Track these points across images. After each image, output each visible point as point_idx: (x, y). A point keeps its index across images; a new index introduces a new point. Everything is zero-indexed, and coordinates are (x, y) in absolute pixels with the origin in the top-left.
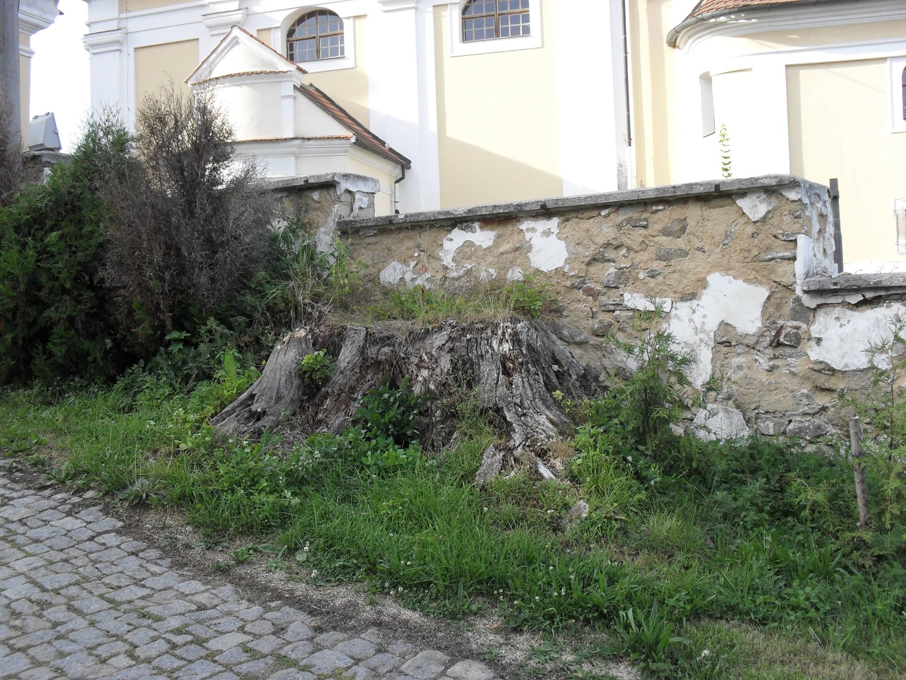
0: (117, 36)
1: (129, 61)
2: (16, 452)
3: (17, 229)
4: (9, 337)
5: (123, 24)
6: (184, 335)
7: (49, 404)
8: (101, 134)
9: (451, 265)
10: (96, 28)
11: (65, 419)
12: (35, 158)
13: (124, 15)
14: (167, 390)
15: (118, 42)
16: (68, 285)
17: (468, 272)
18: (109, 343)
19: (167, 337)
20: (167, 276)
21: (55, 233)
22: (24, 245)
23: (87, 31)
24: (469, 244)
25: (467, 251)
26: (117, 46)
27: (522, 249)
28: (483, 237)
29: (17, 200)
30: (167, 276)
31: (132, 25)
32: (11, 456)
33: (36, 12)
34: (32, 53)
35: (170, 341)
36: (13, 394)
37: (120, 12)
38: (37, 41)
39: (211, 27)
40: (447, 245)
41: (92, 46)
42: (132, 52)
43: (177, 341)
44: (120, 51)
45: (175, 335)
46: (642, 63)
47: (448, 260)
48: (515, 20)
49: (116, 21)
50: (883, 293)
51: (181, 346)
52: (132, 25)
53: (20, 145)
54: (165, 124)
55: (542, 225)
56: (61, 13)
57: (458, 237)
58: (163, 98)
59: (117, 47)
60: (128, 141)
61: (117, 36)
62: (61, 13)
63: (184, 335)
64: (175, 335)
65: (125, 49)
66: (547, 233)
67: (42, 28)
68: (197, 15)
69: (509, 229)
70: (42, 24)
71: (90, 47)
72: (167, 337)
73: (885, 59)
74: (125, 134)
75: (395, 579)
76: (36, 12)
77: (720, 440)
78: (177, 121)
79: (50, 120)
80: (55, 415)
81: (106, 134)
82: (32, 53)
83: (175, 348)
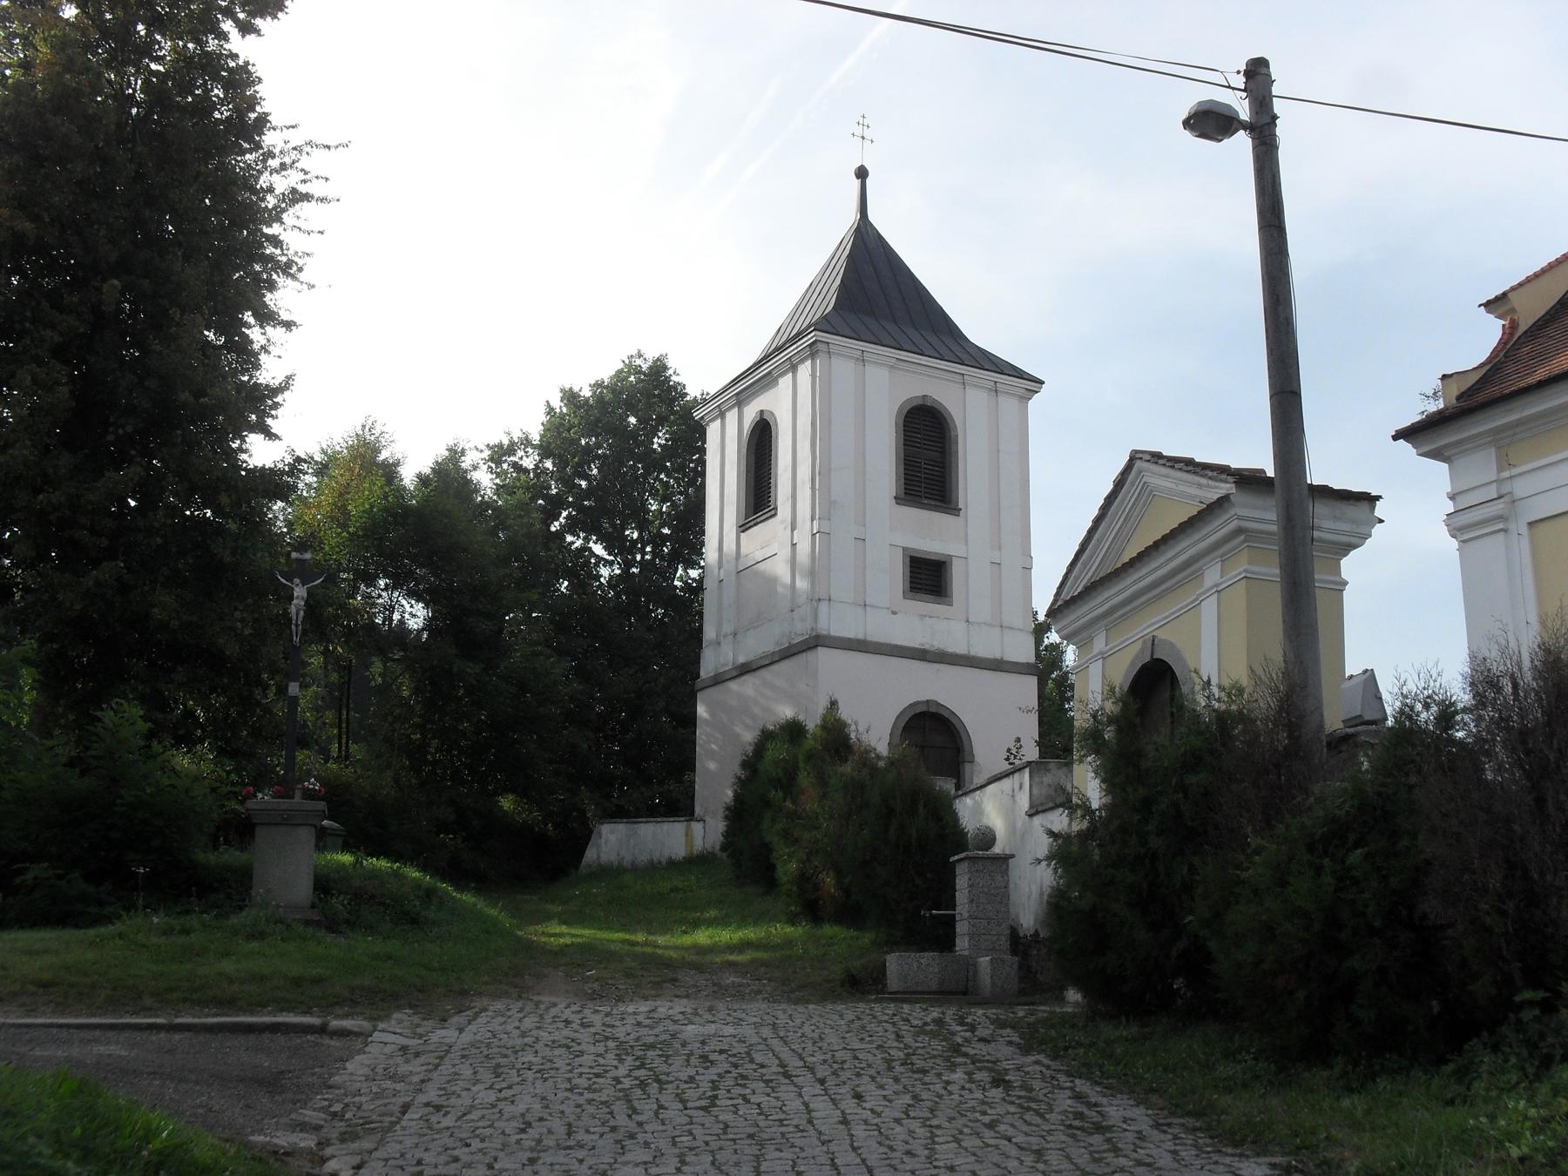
2: (1298, 1148)
3: (1311, 848)
4: (1301, 995)
5: (1506, 488)
6: (1541, 994)
7: (1351, 1090)
8: (1419, 707)
10: (1465, 501)
11: (1368, 1112)
12: (1346, 738)
13: (1506, 474)
14: (1514, 1078)
15: (1500, 518)
16: (1377, 924)
18: (1436, 1006)
19: (1517, 999)
20: (1510, 906)
21: (1359, 851)
22: (1319, 870)
23: (1450, 507)
26: (1499, 523)
29: (1309, 808)
30: (1510, 906)
32: (1290, 1153)
33: (1345, 527)
34: (1346, 583)
35: (1522, 1002)
36: (1306, 1075)
37: (1500, 469)
38: (1350, 565)
42: (1524, 530)
43: (1531, 1003)
44: (1505, 530)
45: (1528, 995)
51: (1537, 1012)
52: (1521, 488)
53: (1321, 726)
54: (1498, 689)
56: (1381, 521)
58: (1495, 654)
59: (1501, 526)
60: (1456, 712)
61: (1498, 508)
62: (1381, 521)
63: (1541, 994)
64: (1528, 995)
65: (1512, 526)
67: (1355, 547)
70: (1354, 540)
71: (1455, 531)
72: (1517, 999)
74: (1452, 704)
75: (684, 965)
76: (1345, 527)
77: (1261, 1096)
78: (1515, 686)
79: (1369, 677)
80: (1354, 1104)
81: (1427, 706)
82: (1346, 583)
83: (1527, 1015)
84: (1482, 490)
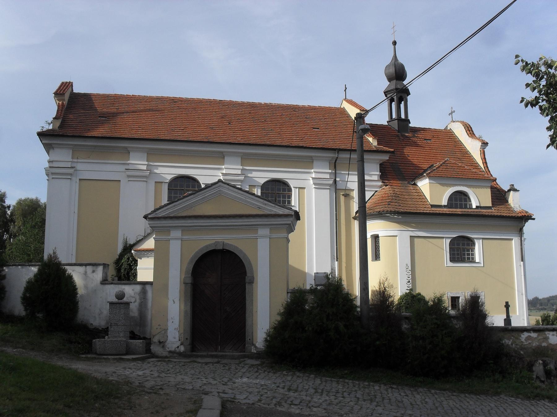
0: (71, 171)
1: (76, 186)
9: (524, 341)
10: (55, 165)
13: (76, 160)
15: (71, 174)
17: (530, 343)
24: (530, 336)
25: (529, 338)
27: (546, 339)
28: (534, 335)
31: (79, 167)
37: (72, 158)
39: (129, 176)
40: (522, 336)
41: (52, 174)
42: (78, 181)
44: (146, 181)
46: (342, 225)
47: (523, 340)
48: (284, 197)
49: (70, 163)
50: (97, 357)
55: (551, 333)
57: (525, 335)
59: (70, 177)
66: (553, 335)
68: (122, 168)
69: (541, 333)
73: (443, 237)
84: (66, 163)
